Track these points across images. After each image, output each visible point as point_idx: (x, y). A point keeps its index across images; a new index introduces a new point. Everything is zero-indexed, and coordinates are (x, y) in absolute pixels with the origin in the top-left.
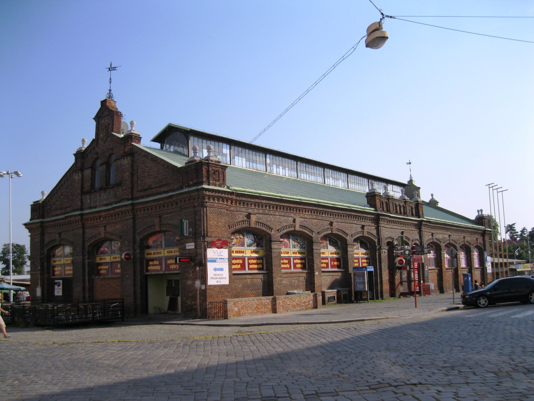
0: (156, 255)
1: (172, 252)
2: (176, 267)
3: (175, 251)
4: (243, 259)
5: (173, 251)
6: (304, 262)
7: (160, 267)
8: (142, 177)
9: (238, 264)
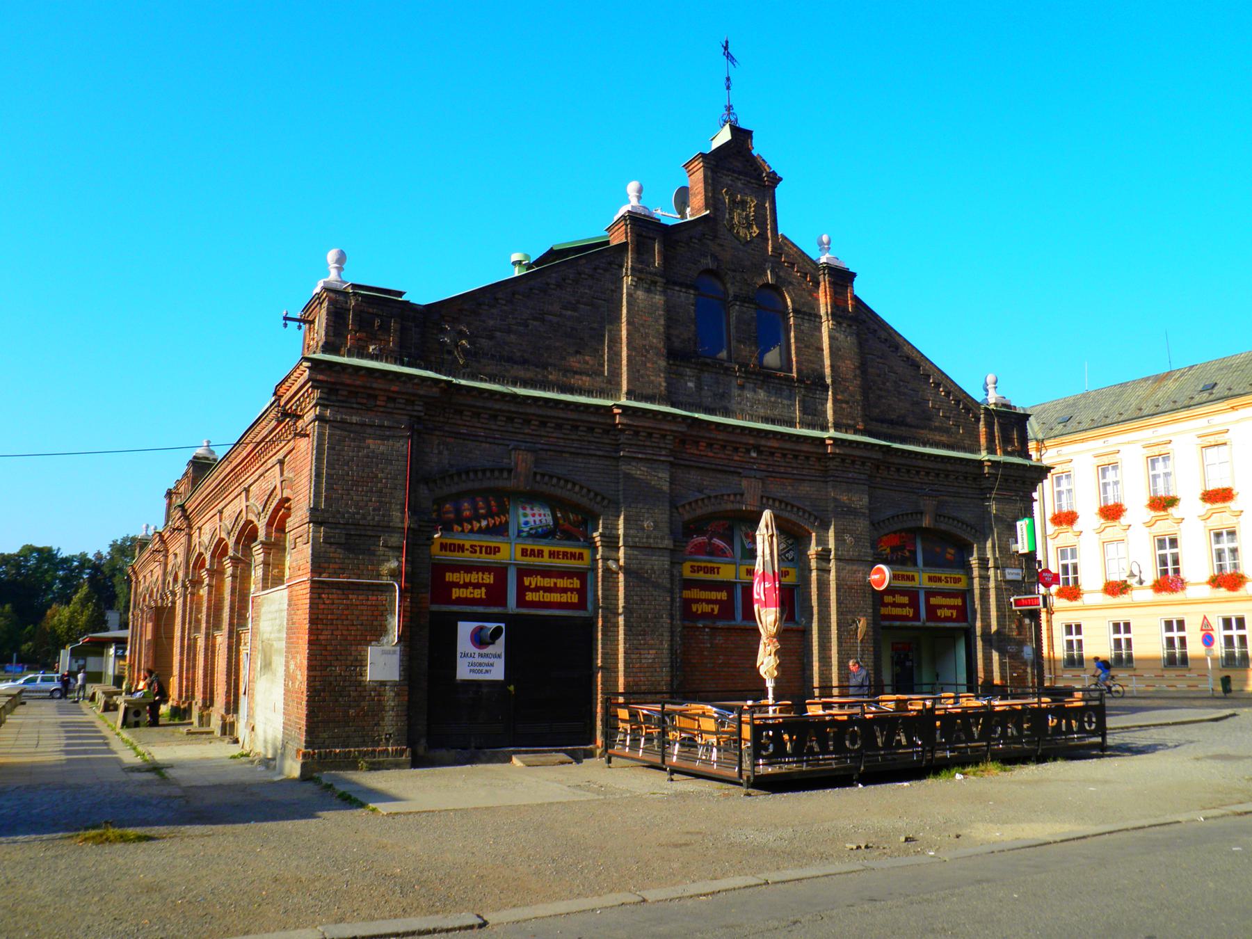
0: (900, 582)
1: (940, 580)
2: (952, 614)
3: (946, 578)
4: (500, 572)
5: (943, 578)
6: (960, 604)
7: (911, 611)
8: (881, 389)
9: (477, 586)
